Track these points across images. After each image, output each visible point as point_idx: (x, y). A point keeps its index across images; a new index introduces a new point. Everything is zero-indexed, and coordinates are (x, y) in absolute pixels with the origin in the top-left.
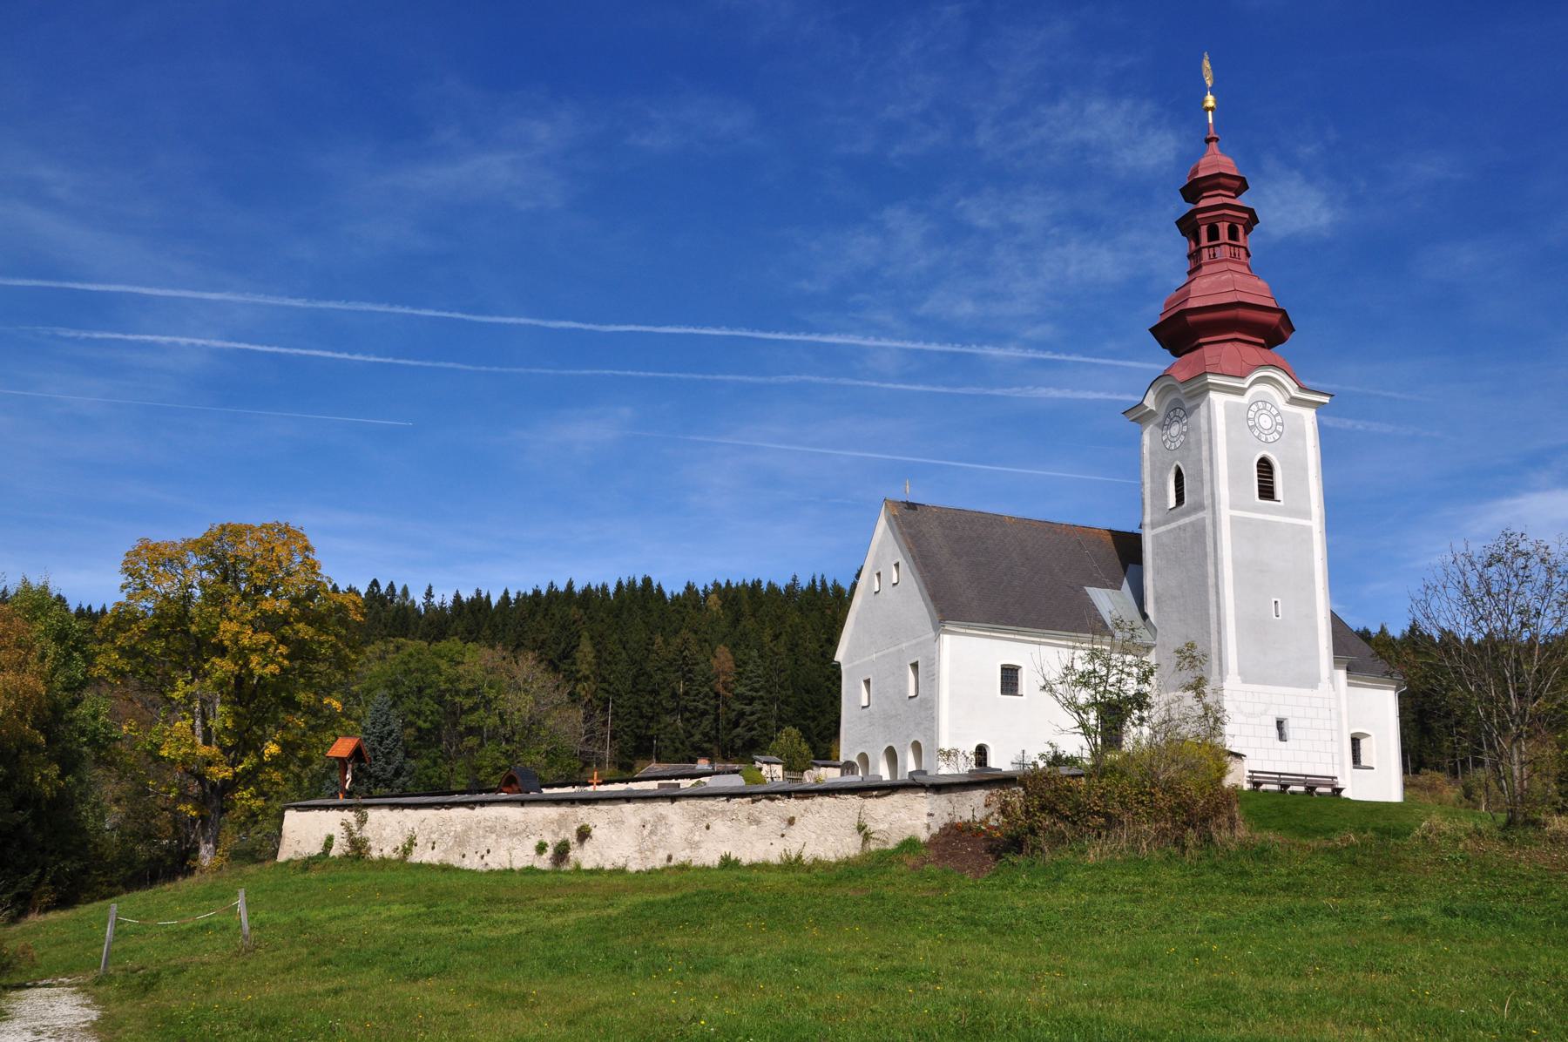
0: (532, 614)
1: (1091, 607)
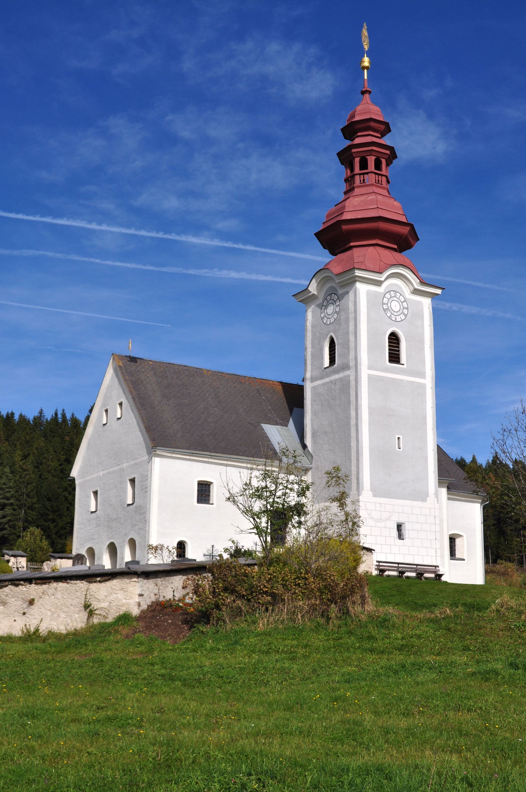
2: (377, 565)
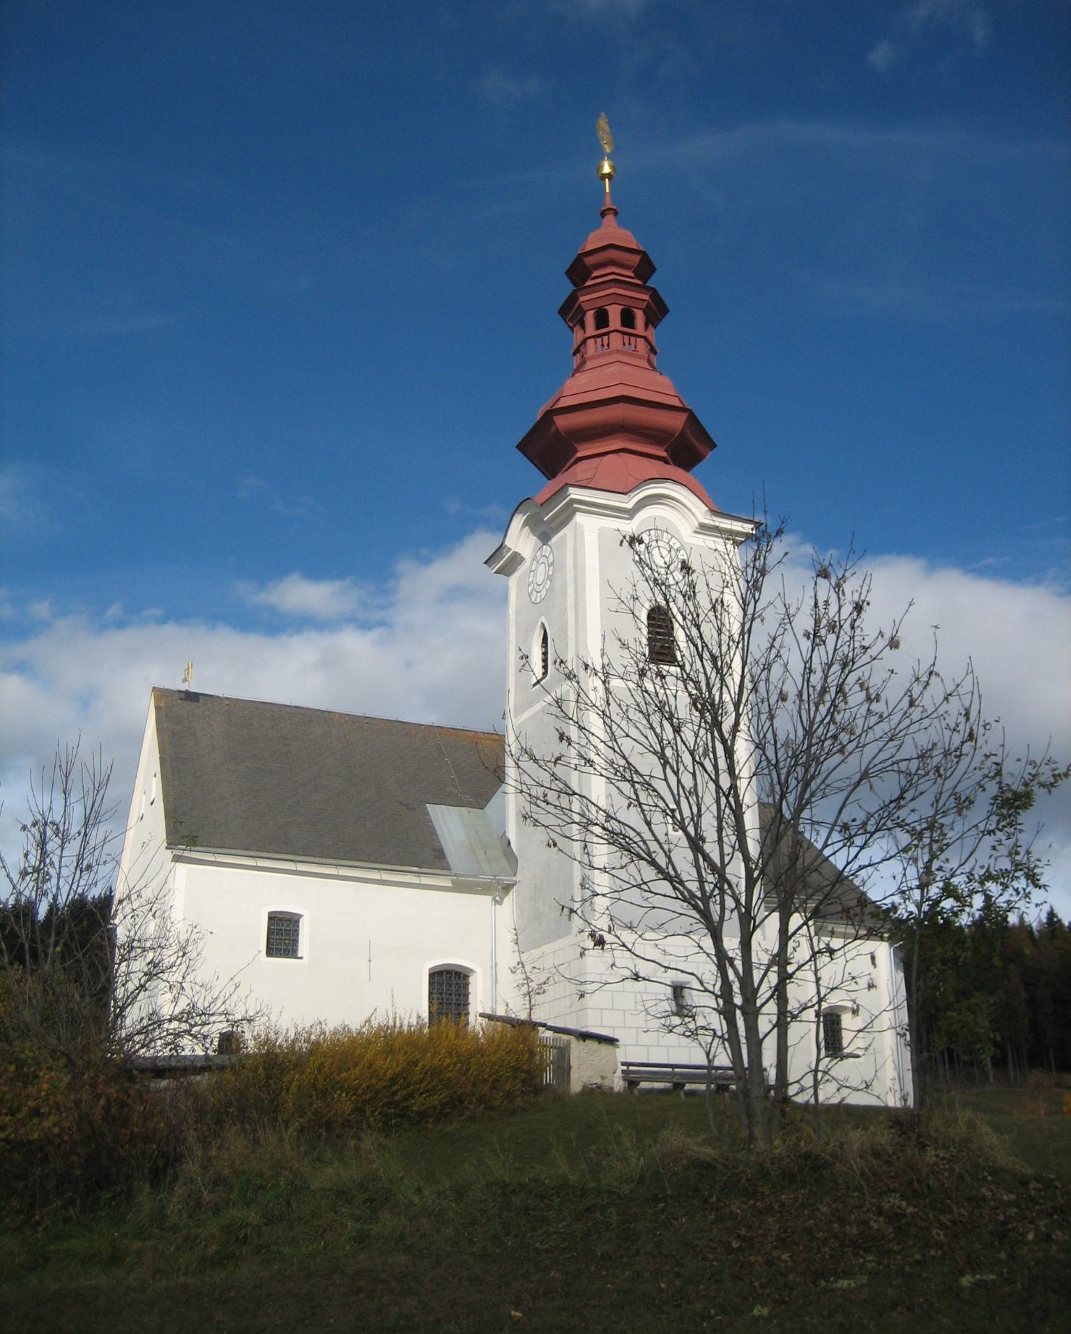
0: (434, 850)
1: (429, 832)
2: (623, 1071)
